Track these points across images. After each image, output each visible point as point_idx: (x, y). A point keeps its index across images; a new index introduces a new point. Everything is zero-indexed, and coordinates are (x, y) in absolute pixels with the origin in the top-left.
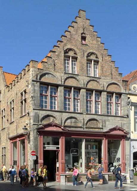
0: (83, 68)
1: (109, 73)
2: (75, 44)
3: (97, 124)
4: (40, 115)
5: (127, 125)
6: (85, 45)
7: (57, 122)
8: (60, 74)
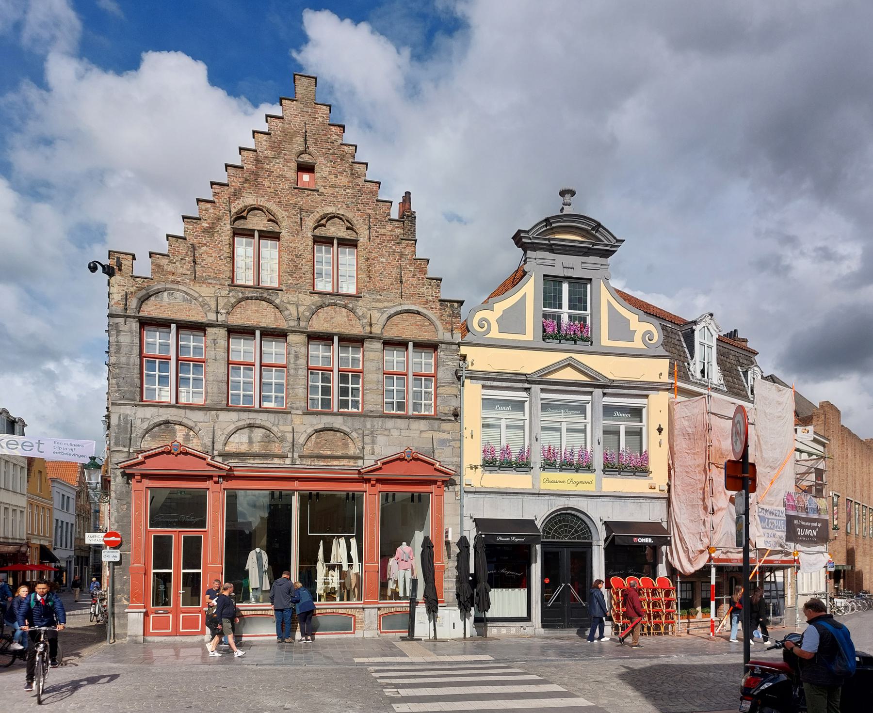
0: (300, 266)
1: (393, 280)
2: (272, 190)
3: (346, 445)
4: (138, 422)
5: (452, 443)
6: (306, 192)
7: (195, 445)
8: (212, 290)
